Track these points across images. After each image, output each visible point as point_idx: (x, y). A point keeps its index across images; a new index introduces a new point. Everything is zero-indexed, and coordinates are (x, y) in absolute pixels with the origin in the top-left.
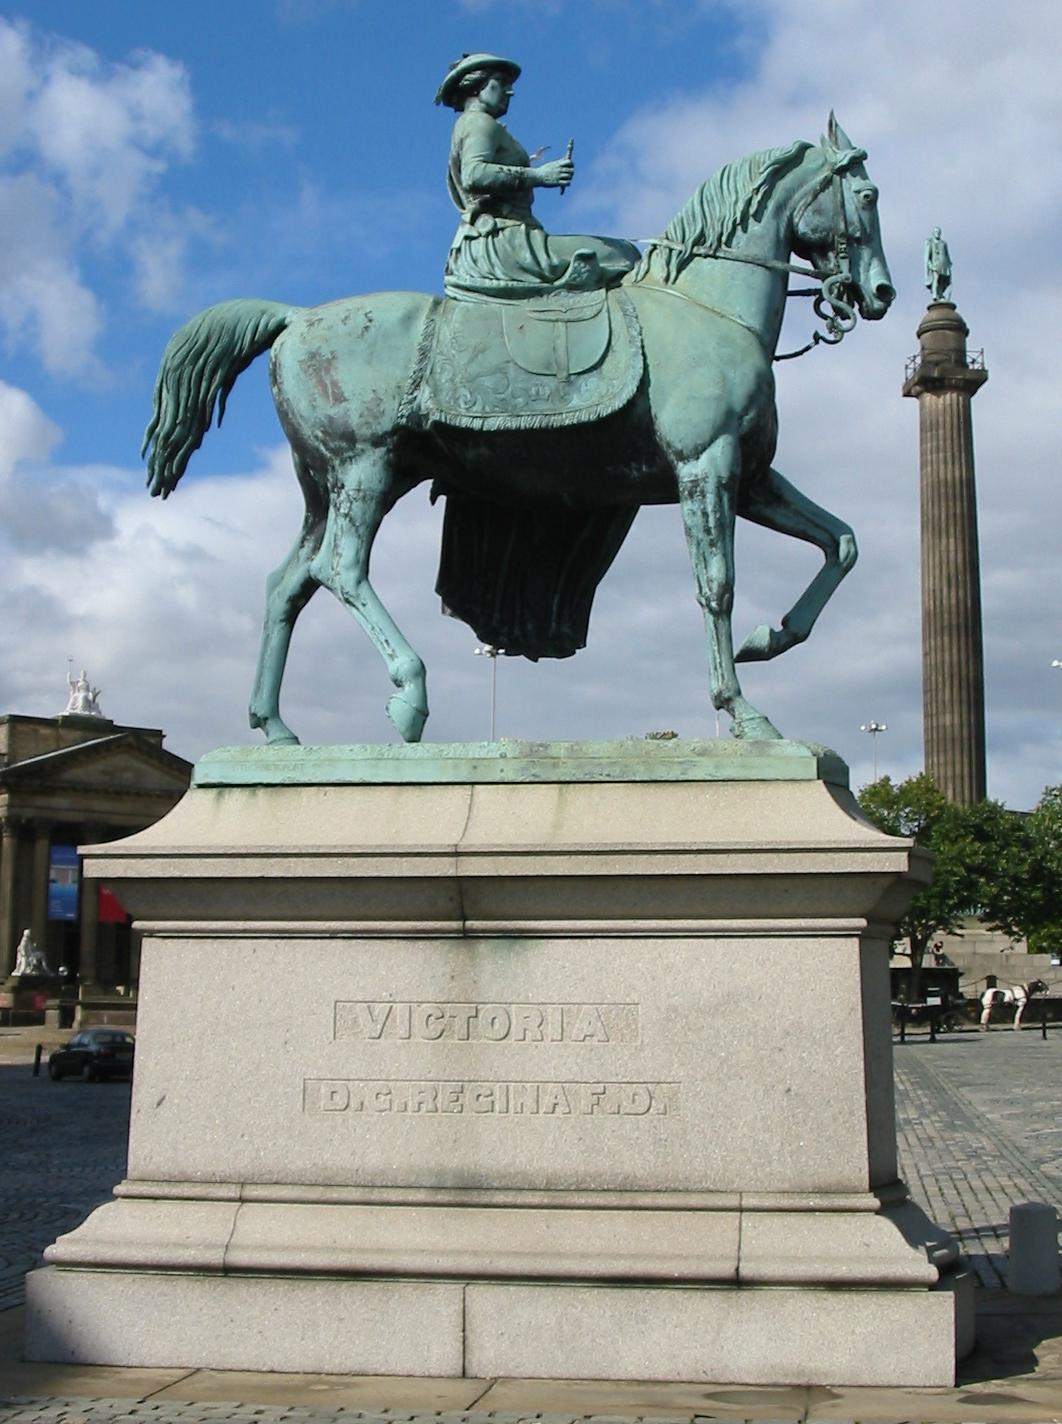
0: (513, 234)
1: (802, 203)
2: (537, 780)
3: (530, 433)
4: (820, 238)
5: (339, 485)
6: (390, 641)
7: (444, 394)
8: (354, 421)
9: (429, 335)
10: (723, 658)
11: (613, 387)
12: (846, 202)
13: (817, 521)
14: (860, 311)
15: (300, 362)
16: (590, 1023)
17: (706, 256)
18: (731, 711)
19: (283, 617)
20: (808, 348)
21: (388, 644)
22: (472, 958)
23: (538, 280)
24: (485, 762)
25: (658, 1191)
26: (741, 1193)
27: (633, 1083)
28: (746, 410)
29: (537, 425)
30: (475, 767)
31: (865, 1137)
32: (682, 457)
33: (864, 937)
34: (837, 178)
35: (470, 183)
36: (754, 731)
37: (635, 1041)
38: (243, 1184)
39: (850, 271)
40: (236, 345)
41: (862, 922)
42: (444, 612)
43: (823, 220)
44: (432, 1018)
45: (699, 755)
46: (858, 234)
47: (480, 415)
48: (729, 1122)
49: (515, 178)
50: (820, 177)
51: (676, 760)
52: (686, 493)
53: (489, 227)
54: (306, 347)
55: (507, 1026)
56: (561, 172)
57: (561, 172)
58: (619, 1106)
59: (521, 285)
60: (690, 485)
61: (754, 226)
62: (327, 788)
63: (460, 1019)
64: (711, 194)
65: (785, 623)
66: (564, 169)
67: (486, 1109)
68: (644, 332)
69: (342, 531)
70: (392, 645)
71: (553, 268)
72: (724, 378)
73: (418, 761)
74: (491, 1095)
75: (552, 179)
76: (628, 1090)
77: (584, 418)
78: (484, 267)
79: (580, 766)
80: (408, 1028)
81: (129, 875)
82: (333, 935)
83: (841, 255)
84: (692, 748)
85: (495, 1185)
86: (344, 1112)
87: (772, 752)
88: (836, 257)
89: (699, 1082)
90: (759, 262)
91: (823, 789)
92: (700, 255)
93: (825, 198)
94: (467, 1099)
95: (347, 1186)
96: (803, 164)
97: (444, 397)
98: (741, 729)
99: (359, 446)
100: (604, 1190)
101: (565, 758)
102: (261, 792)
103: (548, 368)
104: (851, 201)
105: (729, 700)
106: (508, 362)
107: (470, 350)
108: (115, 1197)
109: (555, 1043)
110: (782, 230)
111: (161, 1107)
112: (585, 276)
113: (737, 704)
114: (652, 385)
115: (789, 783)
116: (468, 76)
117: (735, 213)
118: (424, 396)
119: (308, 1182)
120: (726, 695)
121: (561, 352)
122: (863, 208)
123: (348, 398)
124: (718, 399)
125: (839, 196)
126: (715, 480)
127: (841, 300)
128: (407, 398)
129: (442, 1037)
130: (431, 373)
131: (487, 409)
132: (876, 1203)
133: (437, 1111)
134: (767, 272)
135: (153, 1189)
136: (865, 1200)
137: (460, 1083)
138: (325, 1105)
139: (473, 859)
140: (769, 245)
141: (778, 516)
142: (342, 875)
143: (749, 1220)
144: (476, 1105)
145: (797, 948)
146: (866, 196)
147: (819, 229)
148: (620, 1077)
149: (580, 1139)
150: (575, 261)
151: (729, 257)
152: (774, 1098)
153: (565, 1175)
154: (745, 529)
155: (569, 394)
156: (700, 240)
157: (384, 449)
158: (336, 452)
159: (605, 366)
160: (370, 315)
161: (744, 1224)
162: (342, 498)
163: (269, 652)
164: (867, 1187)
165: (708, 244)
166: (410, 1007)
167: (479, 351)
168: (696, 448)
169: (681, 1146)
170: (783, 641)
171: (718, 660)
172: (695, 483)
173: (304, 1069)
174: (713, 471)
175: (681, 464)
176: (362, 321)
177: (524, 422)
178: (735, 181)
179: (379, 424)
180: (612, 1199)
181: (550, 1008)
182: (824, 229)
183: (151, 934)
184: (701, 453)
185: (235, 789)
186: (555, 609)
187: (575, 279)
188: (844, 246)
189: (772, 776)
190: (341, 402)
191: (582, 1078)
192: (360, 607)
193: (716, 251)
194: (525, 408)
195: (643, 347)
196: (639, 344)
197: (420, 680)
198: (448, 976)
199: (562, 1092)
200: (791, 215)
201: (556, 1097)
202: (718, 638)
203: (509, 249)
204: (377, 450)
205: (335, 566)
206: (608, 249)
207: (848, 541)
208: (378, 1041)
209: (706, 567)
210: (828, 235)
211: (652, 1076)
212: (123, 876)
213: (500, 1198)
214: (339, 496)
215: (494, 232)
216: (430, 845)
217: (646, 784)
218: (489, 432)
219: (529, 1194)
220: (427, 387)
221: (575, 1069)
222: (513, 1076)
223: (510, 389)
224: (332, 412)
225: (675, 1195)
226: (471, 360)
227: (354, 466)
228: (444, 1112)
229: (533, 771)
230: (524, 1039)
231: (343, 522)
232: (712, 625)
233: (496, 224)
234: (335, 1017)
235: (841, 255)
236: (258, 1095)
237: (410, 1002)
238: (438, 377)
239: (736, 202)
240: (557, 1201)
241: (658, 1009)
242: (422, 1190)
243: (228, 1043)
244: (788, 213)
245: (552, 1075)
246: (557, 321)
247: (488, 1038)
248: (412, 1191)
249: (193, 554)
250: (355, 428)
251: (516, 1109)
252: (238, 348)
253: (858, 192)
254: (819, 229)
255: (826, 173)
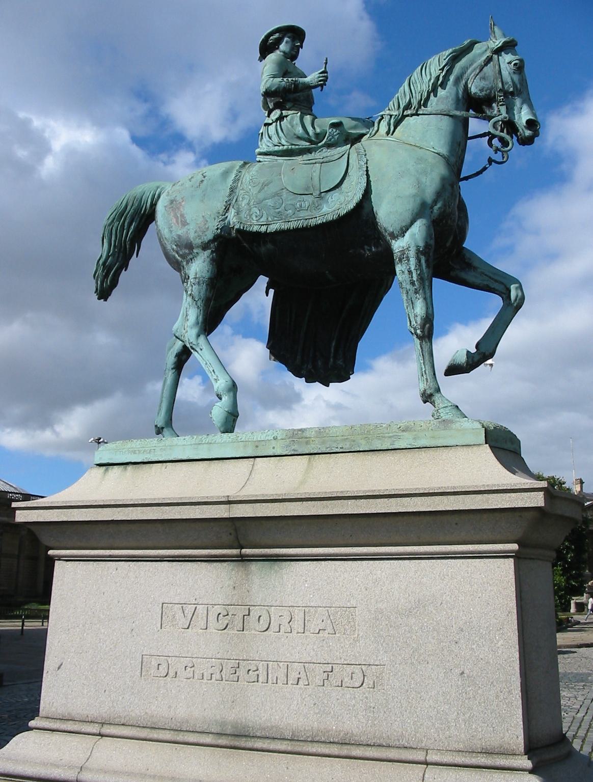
0: (292, 119)
1: (472, 75)
2: (296, 453)
3: (296, 230)
4: (485, 94)
5: (187, 277)
6: (215, 371)
7: (244, 213)
8: (192, 236)
9: (236, 180)
10: (427, 368)
11: (348, 196)
12: (502, 71)
13: (496, 278)
14: (518, 140)
15: (165, 207)
16: (323, 621)
17: (412, 115)
18: (433, 403)
19: (172, 367)
20: (485, 169)
21: (214, 372)
22: (247, 575)
23: (308, 144)
24: (263, 443)
25: (368, 745)
26: (427, 750)
27: (352, 665)
28: (435, 202)
29: (301, 226)
30: (257, 446)
31: (520, 711)
32: (394, 236)
33: (517, 557)
34: (495, 56)
35: (264, 90)
36: (445, 414)
37: (354, 634)
38: (103, 724)
39: (507, 113)
40: (143, 206)
41: (515, 547)
42: (270, 359)
43: (487, 83)
44: (221, 615)
45: (403, 431)
46: (511, 89)
47: (265, 223)
48: (419, 696)
49: (292, 84)
50: (484, 58)
51: (387, 435)
52: (397, 260)
53: (277, 116)
54: (169, 197)
55: (269, 621)
56: (319, 77)
57: (319, 77)
58: (342, 681)
59: (297, 147)
60: (399, 254)
61: (442, 92)
62: (168, 464)
63: (238, 617)
64: (415, 78)
65: (477, 346)
66: (321, 75)
67: (254, 680)
68: (368, 162)
69: (190, 306)
70: (216, 373)
71: (317, 135)
72: (419, 182)
73: (223, 444)
74: (257, 670)
75: (314, 82)
76: (348, 669)
77: (330, 218)
78: (275, 139)
79: (323, 443)
80: (205, 622)
81: (39, 520)
82: (161, 559)
83: (501, 103)
84: (398, 427)
85: (258, 734)
86: (165, 678)
87: (454, 426)
88: (498, 106)
89: (398, 665)
90: (445, 113)
91: (489, 450)
92: (408, 116)
93: (488, 70)
94: (242, 672)
95: (165, 729)
96: (474, 50)
97: (243, 215)
98: (438, 415)
99: (195, 251)
100: (331, 742)
101: (314, 437)
102: (130, 468)
103: (307, 190)
104: (505, 69)
105: (431, 395)
106: (282, 189)
107: (260, 185)
108: (31, 729)
109: (299, 634)
110: (461, 93)
111: (60, 670)
112: (336, 137)
113: (437, 398)
114: (373, 193)
115: (465, 448)
116: (271, 38)
117: (429, 86)
118: (232, 217)
119: (142, 725)
120: (428, 392)
121: (316, 179)
122: (514, 73)
123: (188, 222)
124: (415, 196)
125: (497, 67)
126: (415, 248)
127: (503, 132)
128: (222, 218)
129: (226, 630)
130: (236, 201)
131: (270, 219)
132: (528, 764)
133: (222, 680)
134: (451, 118)
135: (51, 724)
136: (520, 762)
137: (238, 661)
138: (154, 673)
139: (240, 505)
140: (451, 102)
141: (470, 277)
142: (159, 518)
143: (431, 771)
144: (246, 677)
145: (468, 567)
146: (515, 64)
147: (485, 89)
148: (343, 660)
149: (315, 704)
150: (329, 129)
151: (426, 113)
152: (452, 679)
153: (305, 730)
154: (438, 284)
155: (321, 205)
156: (408, 106)
157: (209, 251)
158: (182, 256)
159: (343, 186)
160: (204, 174)
161: (426, 776)
162: (188, 285)
163: (166, 389)
164: (523, 751)
165: (413, 108)
166: (208, 607)
167: (265, 185)
168: (401, 229)
169: (385, 712)
170: (476, 358)
171: (424, 370)
172: (403, 252)
173: (142, 648)
174: (413, 243)
175: (393, 241)
176: (200, 177)
177: (292, 225)
178: (430, 69)
179: (206, 235)
180: (335, 750)
181: (296, 610)
182: (488, 89)
183: (60, 558)
184: (406, 232)
185: (115, 466)
186: (332, 350)
187: (331, 139)
188: (502, 97)
189: (455, 444)
190: (185, 226)
191: (317, 660)
192: (199, 351)
193: (417, 111)
194: (293, 216)
195: (367, 171)
196: (365, 169)
197: (231, 394)
198: (232, 587)
199: (303, 669)
200: (466, 83)
201: (299, 673)
202: (423, 355)
203: (289, 127)
204: (206, 252)
205: (186, 327)
206: (354, 123)
207: (517, 288)
208: (187, 630)
209: (413, 308)
210: (491, 92)
211: (365, 660)
212: (37, 521)
213: (259, 744)
214: (187, 284)
215: (281, 118)
216: (212, 497)
217: (366, 453)
218: (271, 233)
219: (279, 742)
220: (233, 210)
221: (312, 653)
222: (271, 658)
223: (283, 205)
224: (180, 232)
225: (380, 749)
226: (259, 192)
227: (194, 264)
228: (226, 681)
229: (293, 447)
230: (279, 632)
231: (189, 299)
232: (419, 346)
233: (282, 113)
234: (162, 614)
235: (501, 103)
236: (115, 665)
237: (208, 604)
238: (240, 203)
239: (430, 79)
240: (298, 749)
241: (369, 611)
242: (210, 735)
243: (99, 629)
244: (464, 82)
245: (296, 657)
246: (316, 163)
247: (256, 631)
248: (204, 735)
249: (338, 407)
250: (192, 240)
251: (272, 680)
252: (143, 209)
253: (510, 63)
254: (485, 89)
255: (488, 54)
